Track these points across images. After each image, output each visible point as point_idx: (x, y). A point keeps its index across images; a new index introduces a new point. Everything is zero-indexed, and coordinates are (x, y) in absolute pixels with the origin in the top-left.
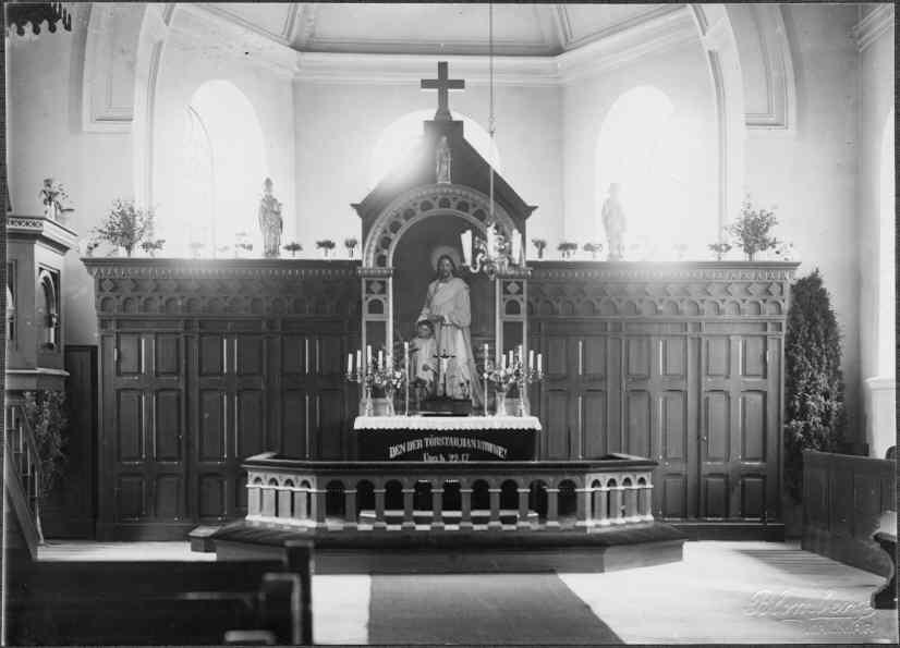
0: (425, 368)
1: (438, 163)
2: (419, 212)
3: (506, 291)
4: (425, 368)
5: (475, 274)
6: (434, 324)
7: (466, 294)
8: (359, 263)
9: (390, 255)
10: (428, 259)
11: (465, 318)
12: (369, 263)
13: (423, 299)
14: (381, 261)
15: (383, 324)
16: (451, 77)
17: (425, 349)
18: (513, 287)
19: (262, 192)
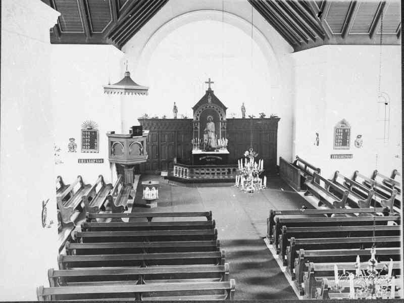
0: (206, 140)
1: (98, 195)
2: (373, 255)
3: (222, 125)
4: (206, 140)
5: (212, 115)
6: (207, 132)
7: (214, 127)
8: (193, 119)
9: (199, 117)
10: (207, 117)
11: (214, 130)
12: (195, 119)
13: (206, 126)
14: (197, 119)
15: (198, 132)
16: (208, 81)
17: (205, 136)
18: (223, 124)
19: (242, 105)
